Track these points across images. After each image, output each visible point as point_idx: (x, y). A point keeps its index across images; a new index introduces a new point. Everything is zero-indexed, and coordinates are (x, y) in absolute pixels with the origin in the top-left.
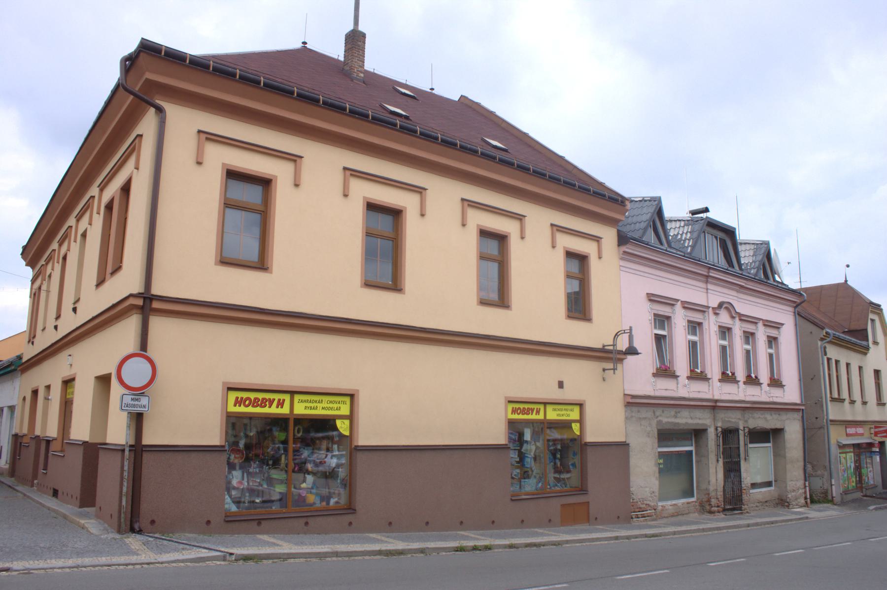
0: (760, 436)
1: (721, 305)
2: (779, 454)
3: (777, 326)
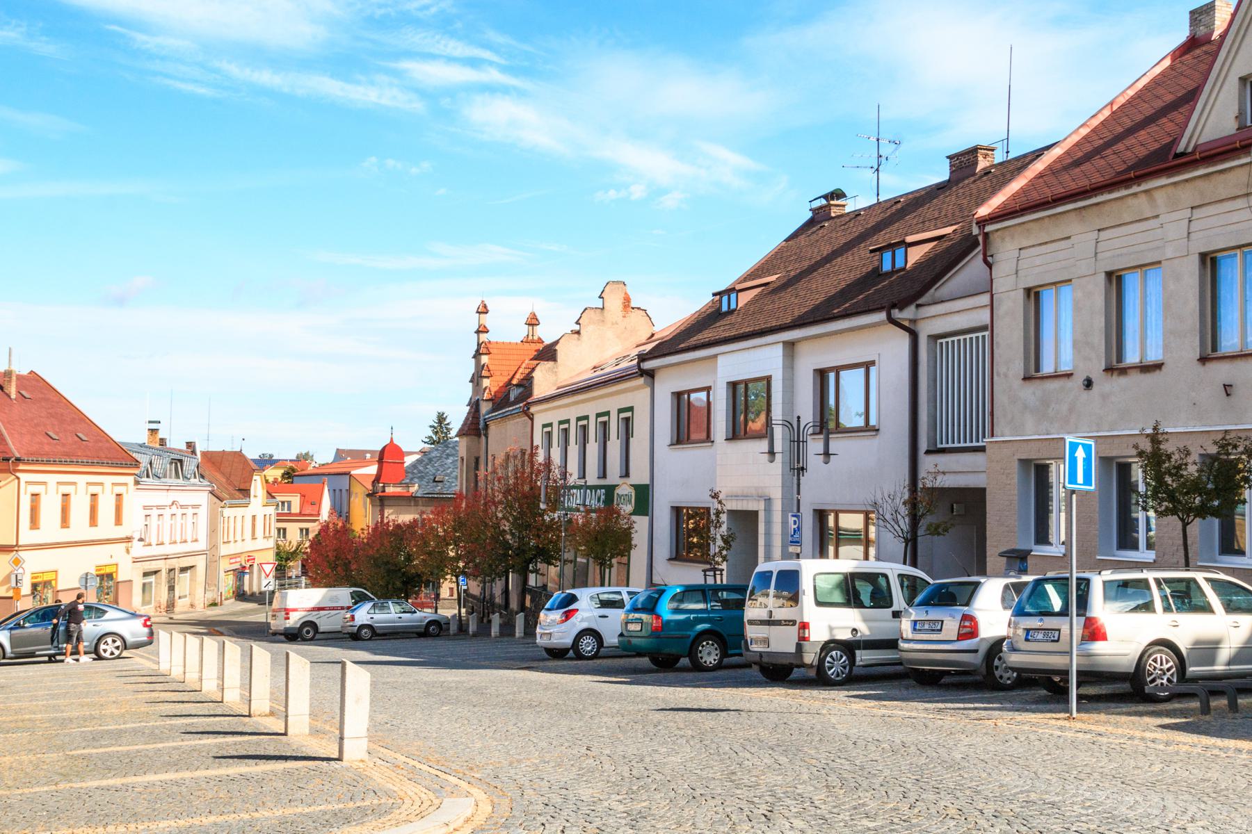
0: (183, 570)
2: (192, 580)
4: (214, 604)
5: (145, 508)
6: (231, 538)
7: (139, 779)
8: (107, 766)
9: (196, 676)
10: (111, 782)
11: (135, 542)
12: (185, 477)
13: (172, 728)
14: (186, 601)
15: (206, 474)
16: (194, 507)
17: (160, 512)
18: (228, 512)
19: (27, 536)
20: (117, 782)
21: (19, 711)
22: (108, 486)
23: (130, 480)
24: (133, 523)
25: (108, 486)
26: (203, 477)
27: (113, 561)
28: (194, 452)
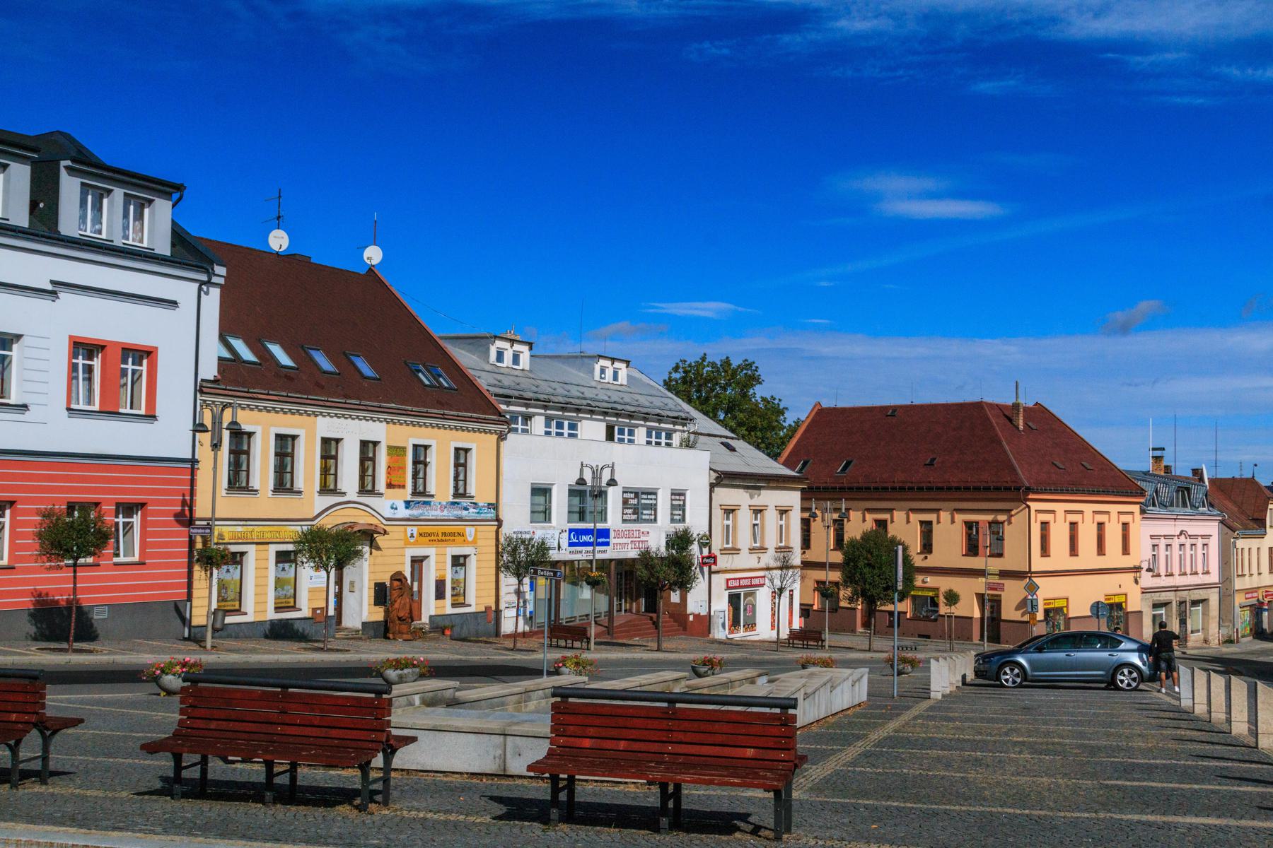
0: (1195, 603)
1: (1181, 533)
2: (1206, 613)
3: (1208, 537)
4: (1229, 641)
5: (1152, 537)
6: (1246, 571)
7: (1180, 819)
8: (1143, 800)
9: (1223, 716)
10: (1151, 818)
11: (1143, 572)
12: (1193, 506)
13: (1206, 769)
14: (1200, 635)
15: (1216, 502)
16: (1203, 537)
17: (1169, 542)
18: (1241, 543)
19: (1039, 564)
20: (1159, 818)
21: (1047, 734)
22: (1060, 514)
23: (1136, 509)
24: (1141, 552)
25: (1060, 514)
26: (1211, 505)
27: (1122, 591)
28: (1201, 479)
